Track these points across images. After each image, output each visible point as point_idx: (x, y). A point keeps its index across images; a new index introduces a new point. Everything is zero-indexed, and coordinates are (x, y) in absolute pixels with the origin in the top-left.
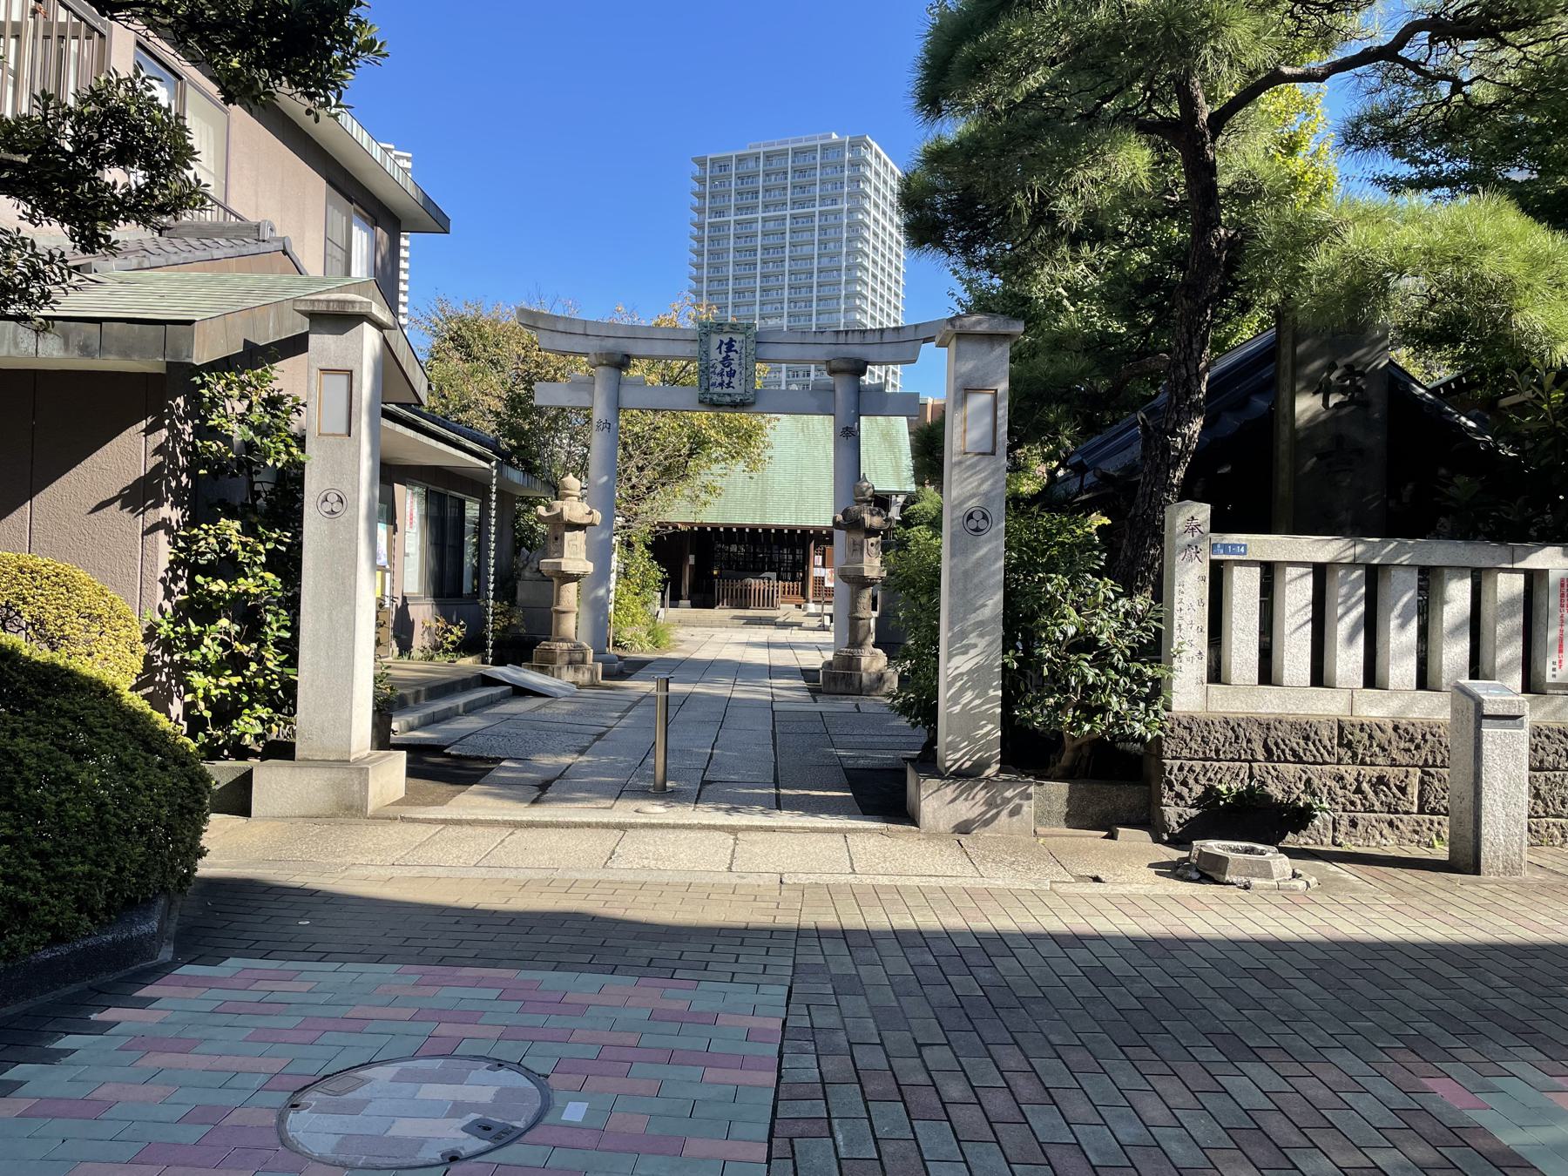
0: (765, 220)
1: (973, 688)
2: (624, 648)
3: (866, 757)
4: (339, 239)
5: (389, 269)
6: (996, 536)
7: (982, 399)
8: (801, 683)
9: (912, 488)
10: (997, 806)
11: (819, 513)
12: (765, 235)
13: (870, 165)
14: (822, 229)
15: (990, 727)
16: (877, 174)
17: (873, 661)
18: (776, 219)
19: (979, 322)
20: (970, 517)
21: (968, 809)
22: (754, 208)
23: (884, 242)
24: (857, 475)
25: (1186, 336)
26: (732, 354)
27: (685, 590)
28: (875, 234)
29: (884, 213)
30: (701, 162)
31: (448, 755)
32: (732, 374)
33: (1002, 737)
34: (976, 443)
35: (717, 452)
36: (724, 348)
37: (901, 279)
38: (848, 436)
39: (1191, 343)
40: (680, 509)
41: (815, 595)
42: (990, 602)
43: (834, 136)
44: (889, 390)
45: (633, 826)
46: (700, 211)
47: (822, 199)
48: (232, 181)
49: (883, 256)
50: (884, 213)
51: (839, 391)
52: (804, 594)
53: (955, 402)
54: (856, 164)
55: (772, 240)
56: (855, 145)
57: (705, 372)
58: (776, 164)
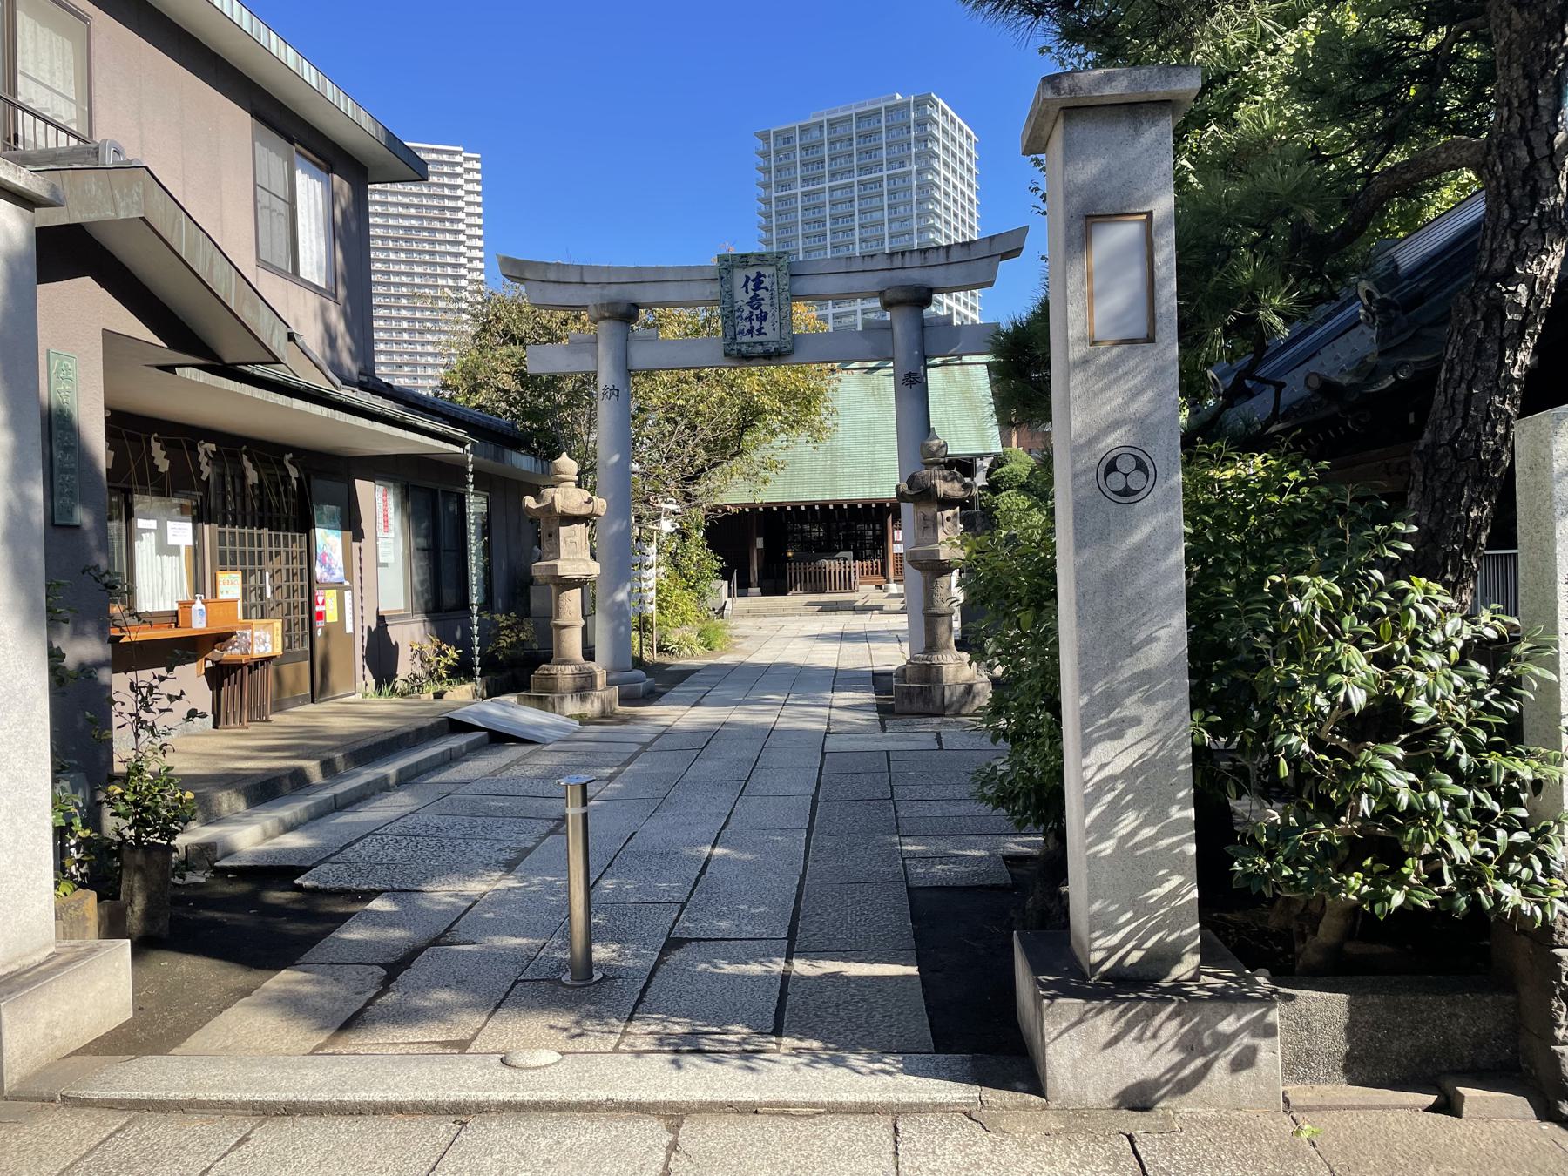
0: (832, 189)
1: (1136, 804)
2: (671, 653)
3: (943, 858)
4: (281, 189)
5: (353, 226)
6: (1166, 503)
7: (1125, 233)
8: (867, 697)
9: (997, 448)
10: (1204, 1052)
11: (884, 486)
12: (833, 204)
13: (937, 123)
14: (891, 193)
15: (1176, 880)
16: (945, 131)
17: (957, 668)
18: (842, 187)
19: (1109, 79)
20: (1111, 467)
21: (1145, 1058)
22: (820, 178)
23: (955, 201)
24: (928, 431)
25: (1522, 85)
27: (754, 577)
28: (947, 194)
29: (954, 171)
30: (765, 137)
31: (299, 888)
32: (763, 317)
33: (1202, 901)
34: (1117, 318)
35: (774, 422)
36: (751, 285)
38: (913, 385)
39: (1534, 95)
40: (735, 489)
41: (896, 573)
42: (1162, 633)
43: (899, 97)
44: (956, 322)
45: (481, 1109)
46: (766, 186)
47: (889, 162)
48: (98, 106)
49: (956, 215)
50: (954, 171)
51: (897, 328)
52: (884, 573)
53: (1069, 243)
54: (922, 123)
55: (840, 209)
56: (921, 104)
57: (730, 316)
58: (840, 131)
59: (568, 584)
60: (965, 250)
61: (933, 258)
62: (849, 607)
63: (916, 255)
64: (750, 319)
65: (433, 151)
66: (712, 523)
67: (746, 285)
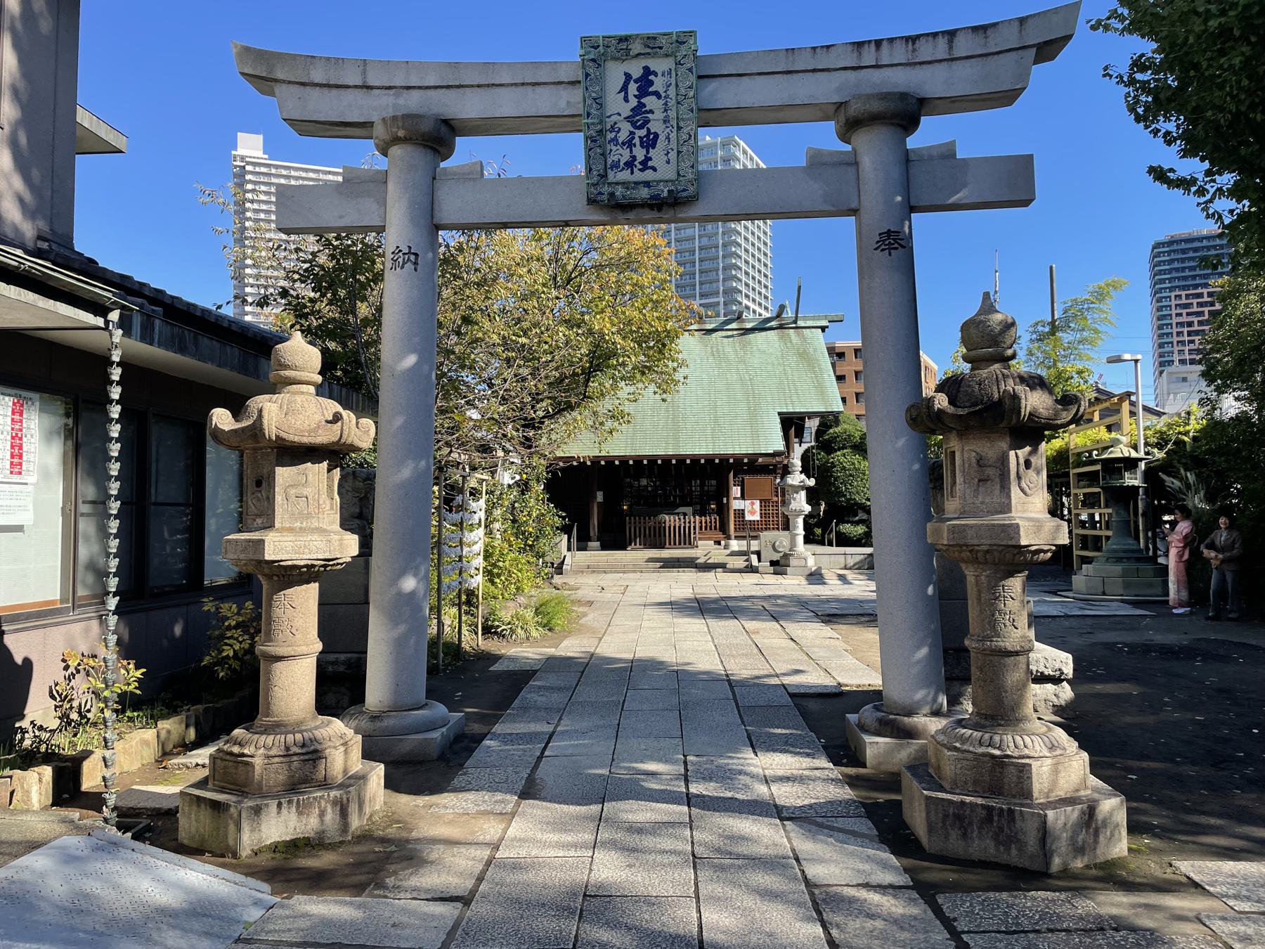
26: (650, 102)
27: (594, 531)
32: (650, 142)
36: (633, 88)
37: (768, 231)
40: (578, 442)
43: (708, 138)
51: (866, 162)
52: (724, 528)
57: (597, 142)
59: (291, 576)
60: (979, 38)
61: (926, 51)
62: (690, 563)
63: (899, 46)
64: (629, 144)
65: (330, 173)
66: (554, 473)
67: (624, 88)
